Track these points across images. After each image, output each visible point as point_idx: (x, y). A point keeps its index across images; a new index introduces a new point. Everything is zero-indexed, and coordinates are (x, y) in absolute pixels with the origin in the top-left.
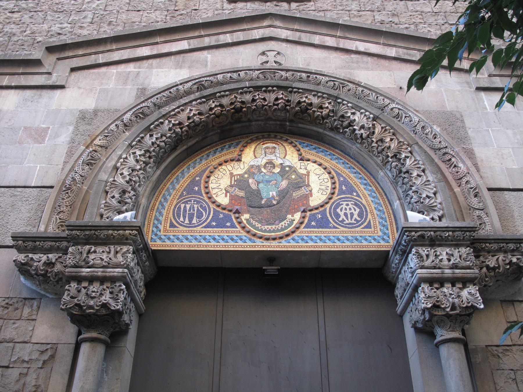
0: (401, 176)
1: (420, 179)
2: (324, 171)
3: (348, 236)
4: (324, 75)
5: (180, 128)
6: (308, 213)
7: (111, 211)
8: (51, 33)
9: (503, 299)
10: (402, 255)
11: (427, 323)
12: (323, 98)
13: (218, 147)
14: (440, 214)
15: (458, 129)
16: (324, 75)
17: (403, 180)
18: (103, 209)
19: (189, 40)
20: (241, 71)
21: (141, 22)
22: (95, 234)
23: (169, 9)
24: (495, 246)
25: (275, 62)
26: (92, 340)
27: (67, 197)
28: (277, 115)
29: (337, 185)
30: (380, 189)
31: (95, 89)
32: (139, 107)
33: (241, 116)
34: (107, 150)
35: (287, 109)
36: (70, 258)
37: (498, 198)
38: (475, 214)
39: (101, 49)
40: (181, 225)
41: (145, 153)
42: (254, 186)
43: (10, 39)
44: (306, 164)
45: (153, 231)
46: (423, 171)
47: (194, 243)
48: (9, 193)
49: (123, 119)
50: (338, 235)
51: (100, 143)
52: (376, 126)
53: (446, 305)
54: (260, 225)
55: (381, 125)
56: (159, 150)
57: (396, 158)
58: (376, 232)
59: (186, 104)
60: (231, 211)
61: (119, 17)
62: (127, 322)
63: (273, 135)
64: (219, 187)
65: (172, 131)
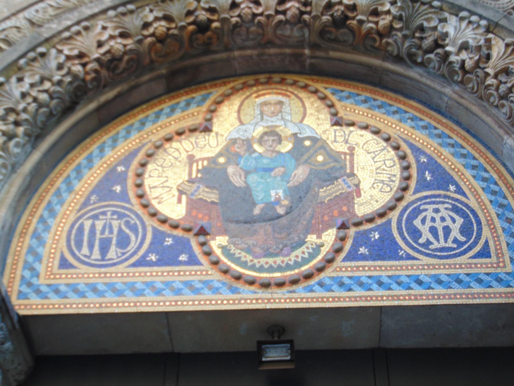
2: (385, 144)
3: (440, 275)
6: (352, 231)
28: (283, 35)
29: (414, 171)
33: (210, 38)
35: (305, 21)
42: (238, 181)
52: (493, 42)
55: (504, 40)
56: (37, 110)
59: (93, 16)
60: (189, 230)
63: (277, 78)
64: (165, 184)
65: (64, 71)
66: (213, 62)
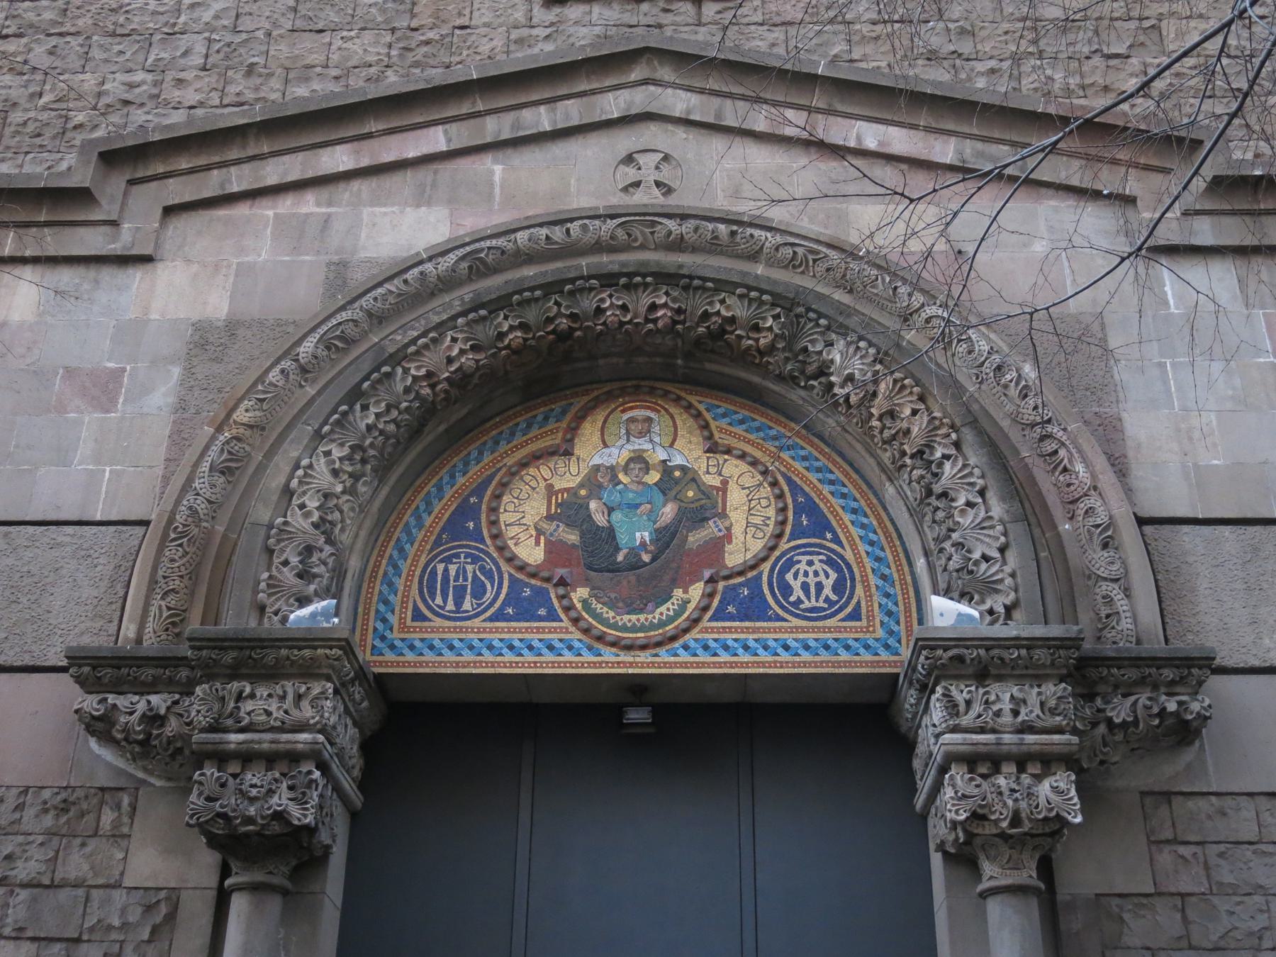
0: (929, 504)
1: (971, 512)
5: (429, 385)
6: (721, 585)
7: (282, 596)
8: (105, 100)
9: (1146, 789)
13: (519, 419)
14: (1008, 602)
16: (770, 229)
18: (264, 592)
19: (447, 126)
20: (571, 220)
21: (327, 66)
22: (250, 657)
23: (396, 25)
24: (1132, 674)
25: (658, 184)
26: (254, 888)
27: (180, 554)
31: (225, 263)
34: (265, 433)
35: (678, 332)
36: (199, 712)
37: (1165, 544)
38: (1098, 590)
39: (234, 154)
42: (600, 519)
43: (6, 118)
45: (375, 629)
46: (982, 493)
47: (468, 656)
48: (45, 539)
49: (298, 355)
50: (786, 636)
51: (247, 419)
53: (1001, 814)
54: (613, 614)
57: (922, 459)
58: (871, 629)
61: (272, 53)
62: (325, 843)
65: (412, 396)
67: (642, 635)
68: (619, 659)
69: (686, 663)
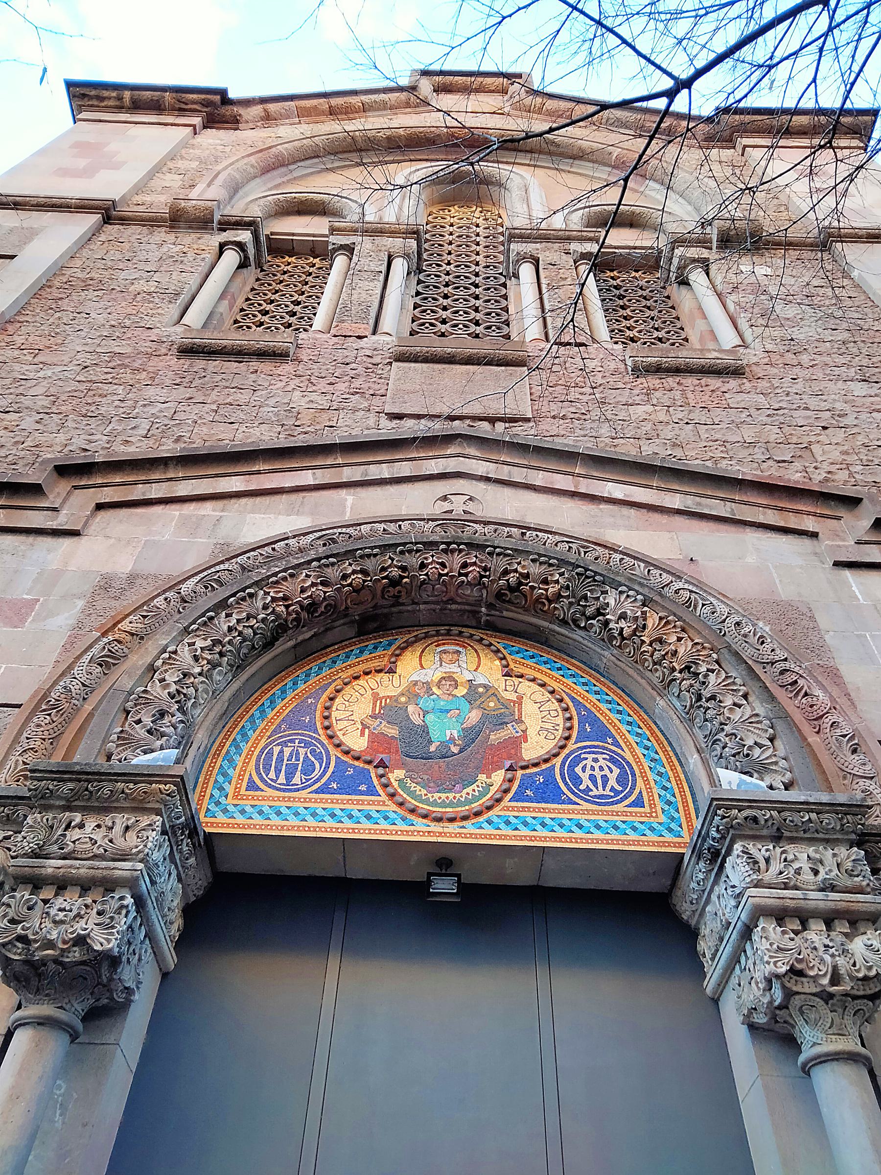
0: (701, 706)
4: (551, 533)
10: (713, 861)
11: (778, 1012)
12: (551, 565)
15: (805, 631)
16: (551, 533)
17: (705, 713)
20: (403, 520)
22: (87, 789)
26: (42, 1022)
30: (659, 734)
32: (213, 570)
33: (400, 592)
35: (484, 583)
38: (856, 787)
40: (270, 786)
41: (214, 645)
42: (417, 720)
44: (516, 684)
50: (579, 817)
57: (689, 672)
63: (455, 630)
66: (400, 612)
67: (451, 810)
68: (429, 829)
69: (490, 835)
